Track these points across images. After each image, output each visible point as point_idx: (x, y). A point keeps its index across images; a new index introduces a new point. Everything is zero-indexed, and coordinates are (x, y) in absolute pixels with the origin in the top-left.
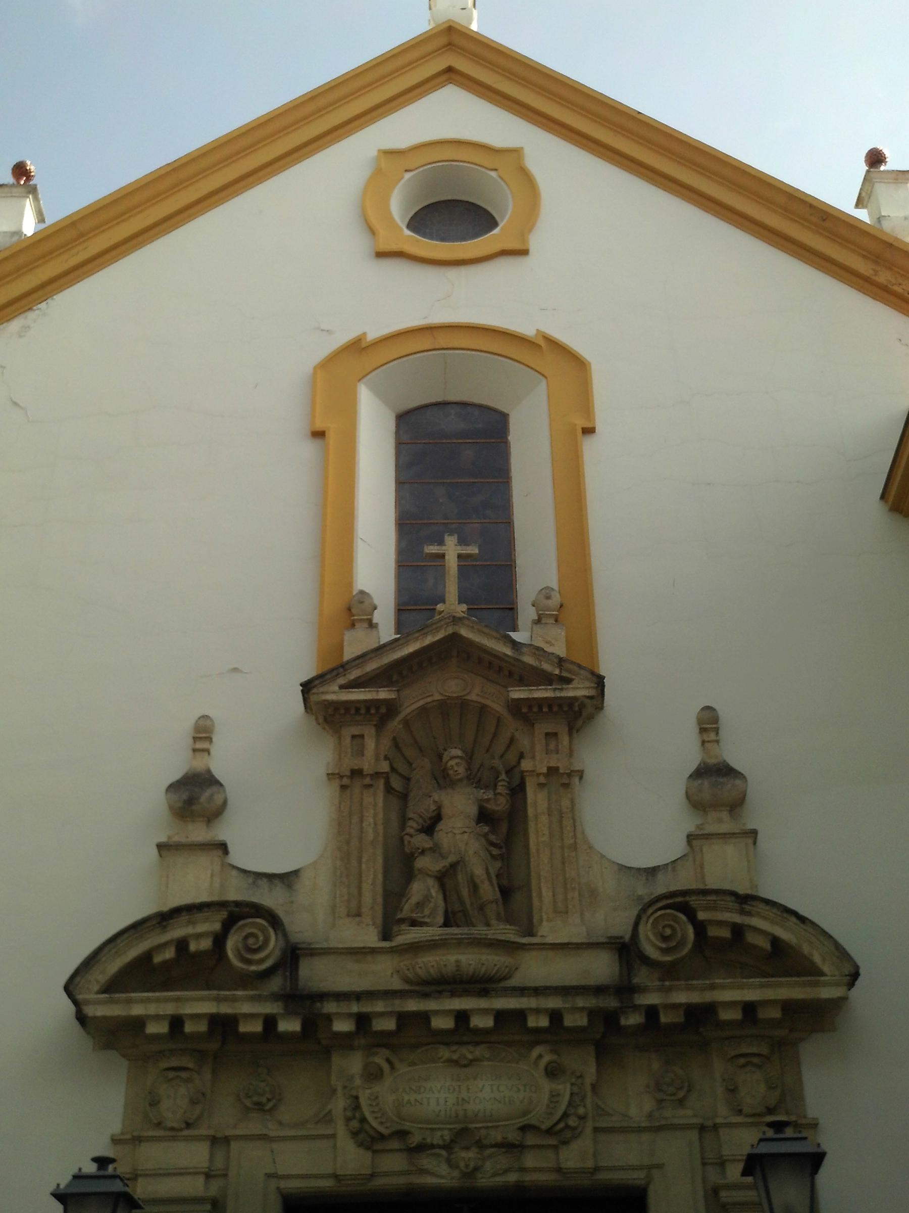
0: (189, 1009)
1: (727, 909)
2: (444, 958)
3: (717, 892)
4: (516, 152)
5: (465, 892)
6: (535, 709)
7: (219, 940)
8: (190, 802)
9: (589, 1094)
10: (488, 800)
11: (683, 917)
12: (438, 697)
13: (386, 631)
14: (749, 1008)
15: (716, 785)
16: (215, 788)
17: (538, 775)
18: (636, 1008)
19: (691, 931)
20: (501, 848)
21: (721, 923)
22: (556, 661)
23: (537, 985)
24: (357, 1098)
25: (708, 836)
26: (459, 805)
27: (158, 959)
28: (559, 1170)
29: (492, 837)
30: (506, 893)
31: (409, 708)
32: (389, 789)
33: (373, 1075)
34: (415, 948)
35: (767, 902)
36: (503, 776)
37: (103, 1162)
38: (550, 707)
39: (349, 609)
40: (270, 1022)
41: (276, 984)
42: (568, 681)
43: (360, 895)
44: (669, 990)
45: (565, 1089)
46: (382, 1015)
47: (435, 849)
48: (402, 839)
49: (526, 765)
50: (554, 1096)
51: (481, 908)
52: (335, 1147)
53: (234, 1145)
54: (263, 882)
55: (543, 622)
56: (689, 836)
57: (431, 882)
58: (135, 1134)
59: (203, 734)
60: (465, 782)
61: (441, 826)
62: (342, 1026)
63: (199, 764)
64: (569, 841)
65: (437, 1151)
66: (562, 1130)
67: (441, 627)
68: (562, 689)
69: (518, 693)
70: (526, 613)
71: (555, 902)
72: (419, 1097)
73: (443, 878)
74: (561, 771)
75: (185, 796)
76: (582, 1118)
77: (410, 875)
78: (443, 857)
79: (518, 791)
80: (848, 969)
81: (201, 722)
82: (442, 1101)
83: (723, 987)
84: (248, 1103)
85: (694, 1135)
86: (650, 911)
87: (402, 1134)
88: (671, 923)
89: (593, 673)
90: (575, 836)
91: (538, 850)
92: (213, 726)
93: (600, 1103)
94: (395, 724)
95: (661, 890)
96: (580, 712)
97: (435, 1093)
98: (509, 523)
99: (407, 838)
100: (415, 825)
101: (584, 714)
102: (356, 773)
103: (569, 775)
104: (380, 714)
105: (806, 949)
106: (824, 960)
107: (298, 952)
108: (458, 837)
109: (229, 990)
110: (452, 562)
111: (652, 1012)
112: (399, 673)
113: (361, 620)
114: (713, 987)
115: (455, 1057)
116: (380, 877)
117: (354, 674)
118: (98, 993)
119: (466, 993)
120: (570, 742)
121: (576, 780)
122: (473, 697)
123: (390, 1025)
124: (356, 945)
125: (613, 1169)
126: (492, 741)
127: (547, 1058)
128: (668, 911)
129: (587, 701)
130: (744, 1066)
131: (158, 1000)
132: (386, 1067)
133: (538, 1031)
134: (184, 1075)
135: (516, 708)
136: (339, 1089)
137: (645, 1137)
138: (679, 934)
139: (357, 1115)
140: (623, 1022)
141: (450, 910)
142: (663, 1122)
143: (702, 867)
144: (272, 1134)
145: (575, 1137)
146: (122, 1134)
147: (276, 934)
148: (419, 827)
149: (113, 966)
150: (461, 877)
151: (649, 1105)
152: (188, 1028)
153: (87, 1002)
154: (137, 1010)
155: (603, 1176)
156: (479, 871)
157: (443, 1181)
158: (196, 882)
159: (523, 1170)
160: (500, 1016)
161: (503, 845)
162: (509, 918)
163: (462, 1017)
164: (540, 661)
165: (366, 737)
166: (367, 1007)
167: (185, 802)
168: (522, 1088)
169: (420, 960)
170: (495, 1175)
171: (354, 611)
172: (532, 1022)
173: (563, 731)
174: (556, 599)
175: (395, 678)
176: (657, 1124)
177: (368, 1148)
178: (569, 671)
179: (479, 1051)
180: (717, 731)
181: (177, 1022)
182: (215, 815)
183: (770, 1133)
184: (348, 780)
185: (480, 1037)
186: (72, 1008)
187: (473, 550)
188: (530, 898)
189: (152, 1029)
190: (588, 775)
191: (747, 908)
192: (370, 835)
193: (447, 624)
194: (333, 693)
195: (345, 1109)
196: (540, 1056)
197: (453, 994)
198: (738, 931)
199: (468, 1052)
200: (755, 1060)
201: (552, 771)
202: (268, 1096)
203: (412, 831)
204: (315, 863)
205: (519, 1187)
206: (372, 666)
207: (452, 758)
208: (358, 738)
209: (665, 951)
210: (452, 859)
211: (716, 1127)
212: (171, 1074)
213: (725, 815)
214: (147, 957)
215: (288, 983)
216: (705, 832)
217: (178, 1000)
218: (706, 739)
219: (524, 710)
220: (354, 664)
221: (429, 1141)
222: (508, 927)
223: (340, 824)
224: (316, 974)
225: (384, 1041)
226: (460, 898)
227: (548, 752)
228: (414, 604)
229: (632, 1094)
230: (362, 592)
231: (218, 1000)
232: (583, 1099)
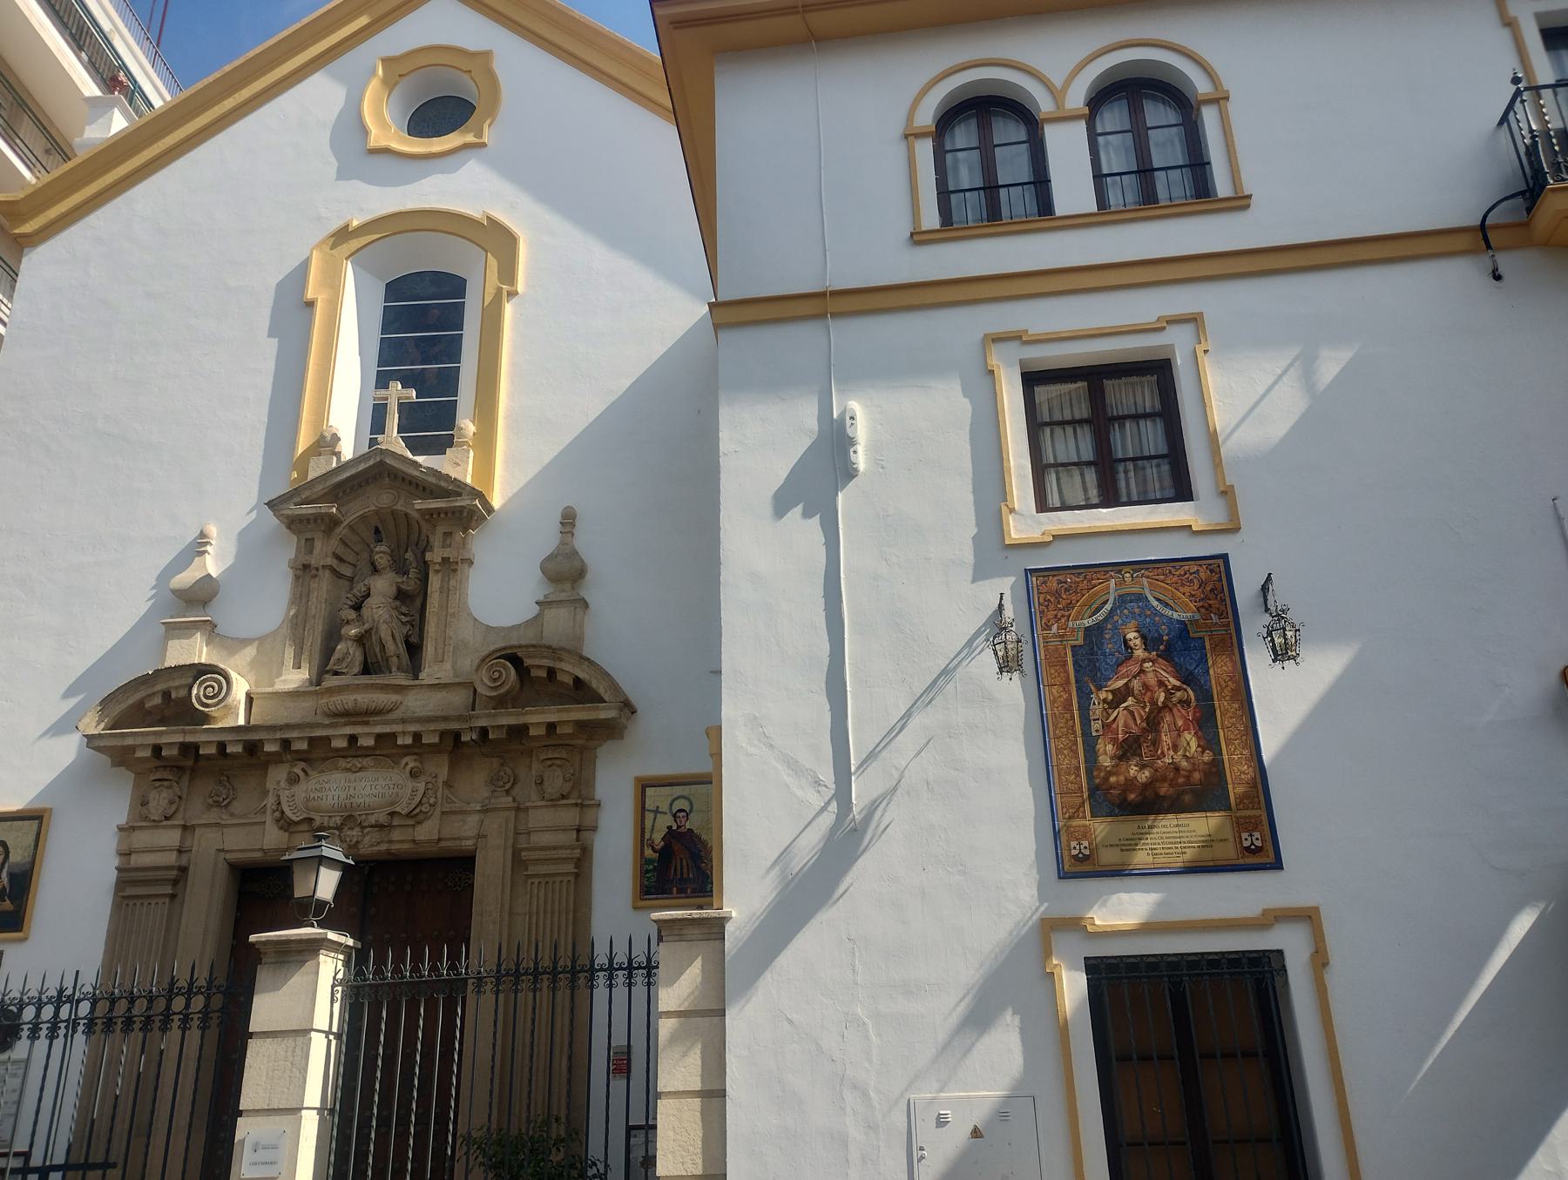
4: (487, 55)
14: (551, 727)
21: (540, 667)
26: (382, 586)
33: (293, 780)
57: (350, 643)
73: (360, 640)
79: (424, 580)
83: (532, 713)
85: (167, 900)
87: (310, 820)
94: (341, 530)
102: (306, 567)
105: (594, 685)
111: (484, 731)
122: (398, 507)
123: (304, 746)
127: (411, 765)
132: (302, 775)
151: (485, 792)
155: (443, 844)
159: (391, 842)
160: (379, 737)
163: (353, 739)
166: (287, 736)
172: (400, 742)
179: (366, 761)
184: (304, 571)
185: (367, 752)
189: (140, 754)
194: (293, 509)
199: (358, 763)
201: (445, 560)
205: (388, 852)
210: (367, 626)
213: (568, 586)
214: (141, 703)
225: (303, 757)
229: (476, 784)
231: (184, 732)
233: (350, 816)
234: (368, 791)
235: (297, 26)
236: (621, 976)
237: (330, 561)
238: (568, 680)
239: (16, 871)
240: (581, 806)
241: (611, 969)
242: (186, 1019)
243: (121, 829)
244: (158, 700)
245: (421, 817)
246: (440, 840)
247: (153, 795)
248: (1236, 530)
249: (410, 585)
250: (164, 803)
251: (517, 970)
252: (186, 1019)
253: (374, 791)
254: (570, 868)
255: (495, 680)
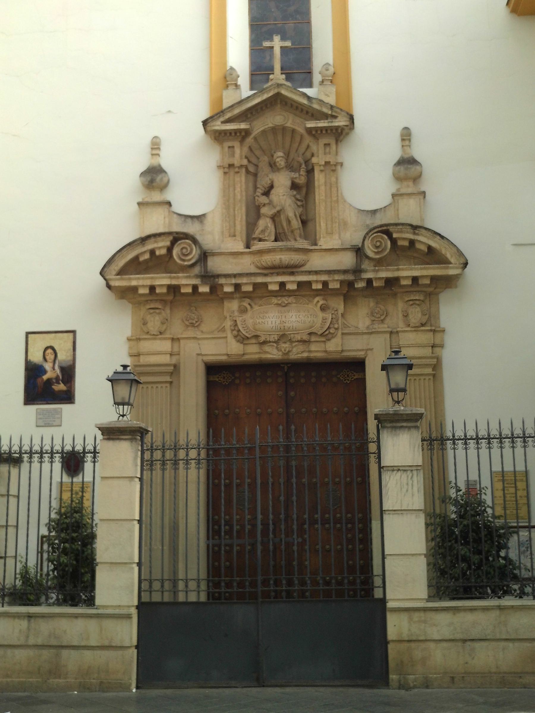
0: (157, 283)
1: (407, 232)
2: (274, 257)
3: (403, 224)
5: (285, 224)
6: (319, 132)
7: (170, 250)
8: (152, 181)
9: (340, 318)
10: (296, 178)
11: (385, 237)
12: (271, 125)
13: (246, 91)
14: (415, 279)
15: (408, 167)
16: (163, 174)
17: (320, 165)
18: (362, 279)
19: (389, 243)
20: (302, 201)
21: (404, 239)
22: (330, 107)
23: (317, 270)
24: (236, 321)
25: (402, 195)
26: (282, 181)
27: (141, 259)
28: (326, 351)
29: (298, 197)
30: (304, 223)
31: (256, 132)
32: (248, 172)
33: (243, 311)
34: (261, 252)
35: (426, 229)
36: (303, 166)
37: (125, 367)
38: (326, 130)
39: (225, 78)
40: (195, 288)
41: (197, 270)
42: (335, 117)
43: (235, 226)
44: (377, 271)
45: (329, 316)
46: (246, 284)
47: (270, 203)
48: (254, 198)
49: (314, 160)
50: (324, 320)
51: (292, 232)
52: (227, 342)
53: (181, 341)
54: (189, 220)
55: (324, 83)
56: (392, 195)
57: (268, 220)
58: (138, 337)
59: (155, 146)
60: (285, 169)
61: (273, 192)
62: (228, 289)
63: (155, 162)
64: (335, 199)
65: (272, 344)
66: (327, 334)
67: (271, 90)
68: (332, 122)
69: (311, 124)
70: (317, 78)
71: (327, 228)
72: (263, 321)
73: (274, 218)
74: (332, 163)
75: (149, 178)
76: (337, 329)
77: (258, 216)
78: (275, 207)
79: (310, 172)
80: (462, 261)
81: (154, 140)
82: (274, 322)
83: (403, 269)
84: (187, 323)
85: (168, 385)
86: (371, 234)
87: (257, 337)
88: (380, 240)
89: (348, 113)
90: (338, 196)
91: (319, 203)
92: (160, 142)
93: (345, 322)
94: (250, 140)
95: (378, 222)
96: (342, 132)
97: (271, 318)
98: (309, 23)
99: (256, 198)
100: (261, 191)
101: (344, 133)
102: (231, 166)
103: (335, 165)
104: (242, 135)
105: (443, 252)
106: (452, 256)
107: (207, 254)
108: (281, 197)
109: (175, 273)
110: (277, 51)
111: (369, 282)
112: (250, 113)
113: (232, 84)
114: (398, 270)
115: (280, 302)
116: (244, 217)
117: (228, 115)
118: (115, 275)
119: (284, 274)
120: (337, 148)
121: (339, 167)
123: (250, 288)
124: (233, 251)
125: (349, 351)
126: (299, 146)
127: (321, 302)
128: (379, 234)
129: (345, 127)
130: (412, 305)
131: (143, 278)
132: (248, 307)
133: (317, 290)
134: (157, 311)
135: (309, 131)
136: (228, 317)
137: (365, 337)
138: (383, 245)
139: (236, 329)
140: (356, 286)
141: (278, 232)
142: (374, 330)
143: (398, 210)
144: (198, 337)
145: (333, 337)
146: (132, 336)
147: (196, 247)
148: (263, 192)
149: (121, 263)
150: (282, 217)
151: (368, 322)
152: (158, 291)
153: (111, 280)
154: (134, 283)
155: (345, 354)
156: (291, 214)
157: (274, 356)
158: (157, 222)
159: (310, 351)
160: (300, 284)
161: (303, 200)
162: (306, 238)
163: (282, 285)
164: (321, 107)
165: (235, 148)
166: (239, 281)
167: (149, 182)
168: (310, 316)
169: (263, 258)
170: (298, 354)
171: (228, 79)
172: (314, 287)
173: (333, 142)
174: (331, 70)
175: (249, 116)
176: (370, 331)
177: (242, 343)
178: (336, 112)
179: (291, 299)
180: (410, 140)
181: (152, 288)
182: (163, 187)
183: (393, 355)
184: (228, 169)
185: (291, 293)
186: (104, 282)
187: (288, 44)
188: (315, 226)
189: (141, 291)
190: (346, 164)
191: (417, 232)
192: (239, 197)
193: (274, 88)
194: (218, 126)
195: (231, 326)
196: (318, 302)
197: (278, 274)
198: (412, 243)
199: (285, 300)
200: (417, 302)
201: (327, 163)
202: (196, 320)
203: (259, 194)
204: (213, 210)
205: (308, 358)
206: (237, 111)
207: (278, 157)
208: (231, 148)
209: (376, 253)
210: (278, 208)
211: (397, 332)
212: (152, 311)
213: (411, 183)
214: (137, 258)
215: (203, 268)
216: (400, 193)
217: (152, 278)
218: (404, 144)
219: (314, 132)
220: (228, 110)
221: (268, 340)
222: (304, 241)
223: (224, 192)
224: (215, 265)
225: (247, 295)
226: (282, 226)
227: (325, 153)
228: (259, 71)
229: (360, 316)
230: (232, 68)
231: (170, 278)
232: (337, 320)
233: (283, 335)
234: (294, 319)
235: (442, 265)
236: (36, 457)
237: (245, 162)
238: (424, 248)
239: (64, 365)
240: (434, 331)
241: (454, 440)
242: (164, 464)
243: (129, 340)
244: (147, 256)
245: (330, 336)
246: (342, 351)
247: (149, 318)
248: (60, 426)
249: (302, 180)
250: (158, 324)
251: (52, 450)
252: (164, 464)
253: (298, 319)
254: (429, 371)
255: (377, 247)
